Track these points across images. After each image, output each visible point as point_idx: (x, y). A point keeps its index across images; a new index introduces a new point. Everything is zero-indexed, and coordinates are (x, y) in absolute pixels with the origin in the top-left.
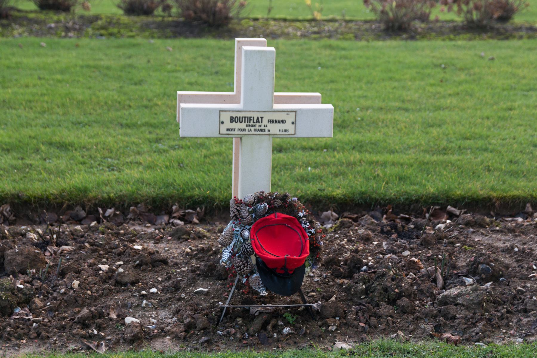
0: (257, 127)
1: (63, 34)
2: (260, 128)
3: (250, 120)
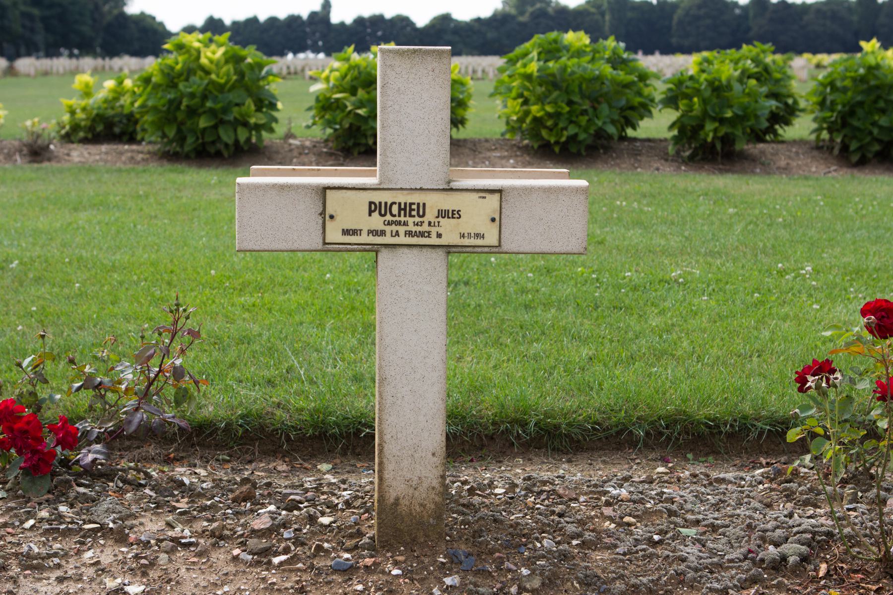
0: (411, 228)
1: (710, 157)
2: (418, 229)
3: (411, 210)
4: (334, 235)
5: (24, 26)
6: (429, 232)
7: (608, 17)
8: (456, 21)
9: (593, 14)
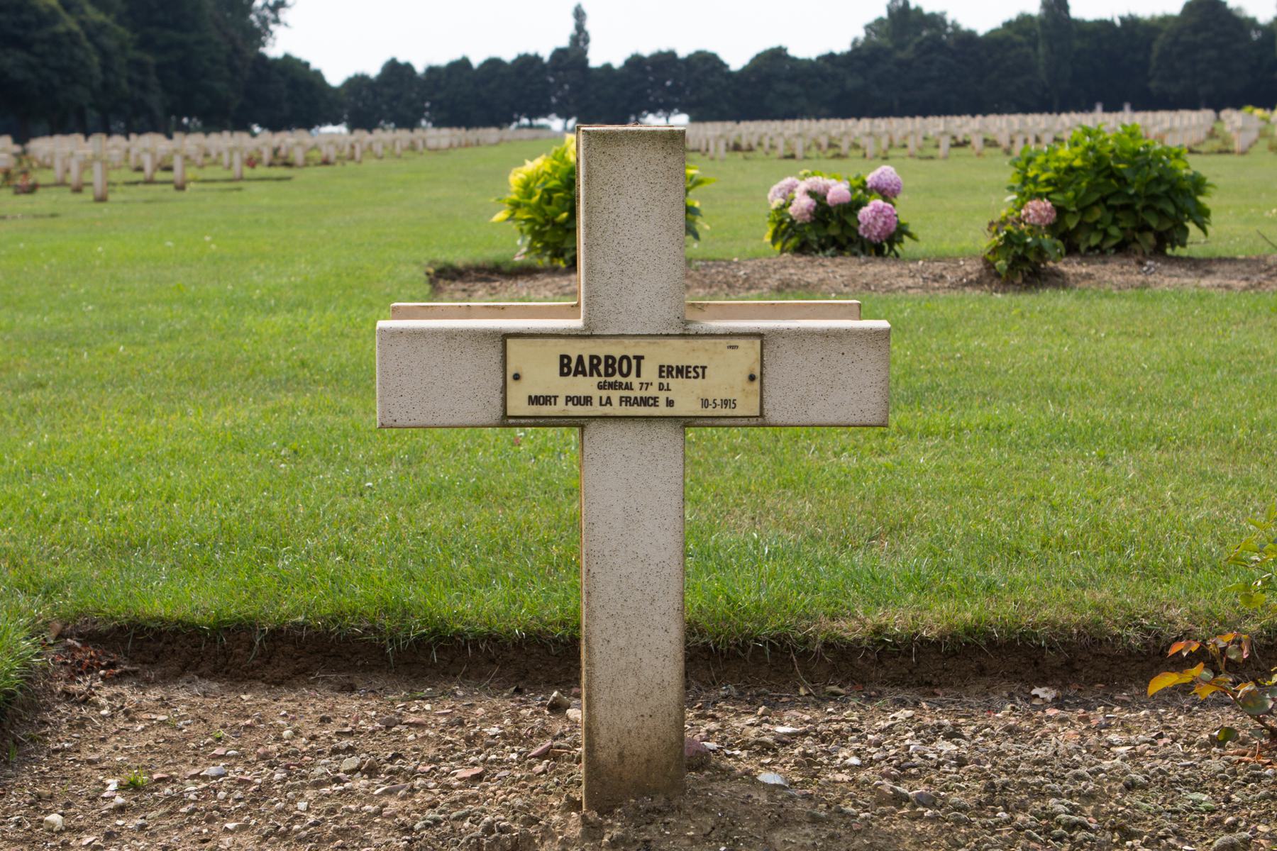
2: (644, 394)
4: (519, 405)
5: (131, 82)
6: (655, 399)
7: (1041, 50)
8: (794, 59)
9: (1021, 45)
